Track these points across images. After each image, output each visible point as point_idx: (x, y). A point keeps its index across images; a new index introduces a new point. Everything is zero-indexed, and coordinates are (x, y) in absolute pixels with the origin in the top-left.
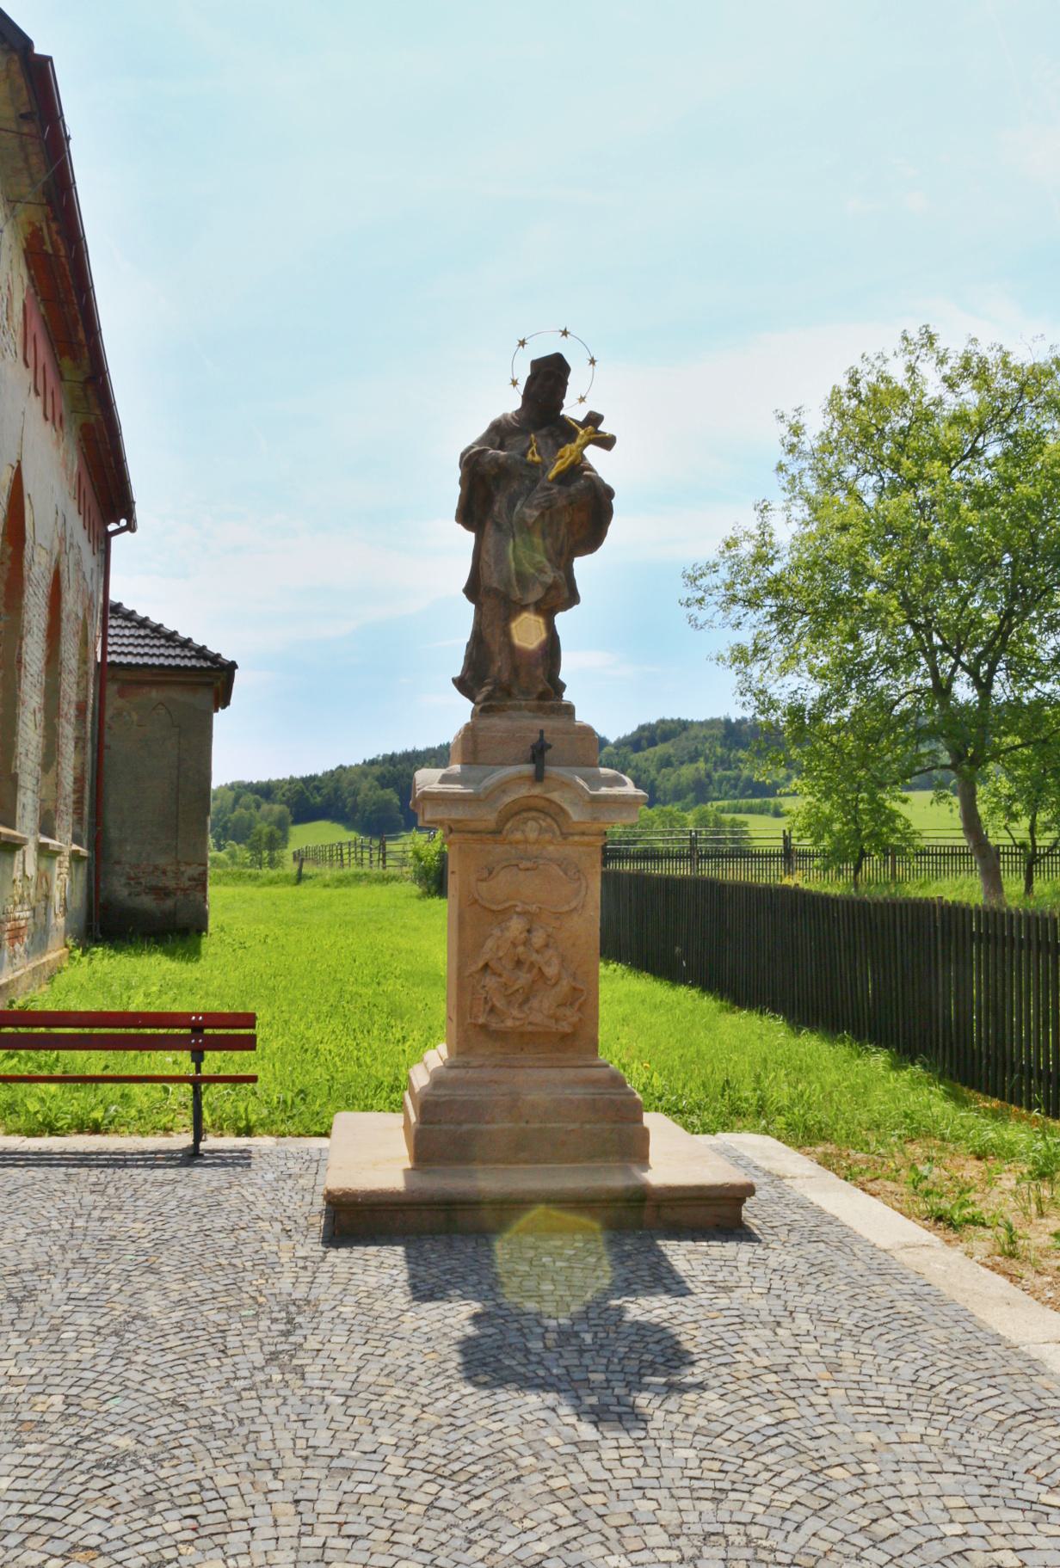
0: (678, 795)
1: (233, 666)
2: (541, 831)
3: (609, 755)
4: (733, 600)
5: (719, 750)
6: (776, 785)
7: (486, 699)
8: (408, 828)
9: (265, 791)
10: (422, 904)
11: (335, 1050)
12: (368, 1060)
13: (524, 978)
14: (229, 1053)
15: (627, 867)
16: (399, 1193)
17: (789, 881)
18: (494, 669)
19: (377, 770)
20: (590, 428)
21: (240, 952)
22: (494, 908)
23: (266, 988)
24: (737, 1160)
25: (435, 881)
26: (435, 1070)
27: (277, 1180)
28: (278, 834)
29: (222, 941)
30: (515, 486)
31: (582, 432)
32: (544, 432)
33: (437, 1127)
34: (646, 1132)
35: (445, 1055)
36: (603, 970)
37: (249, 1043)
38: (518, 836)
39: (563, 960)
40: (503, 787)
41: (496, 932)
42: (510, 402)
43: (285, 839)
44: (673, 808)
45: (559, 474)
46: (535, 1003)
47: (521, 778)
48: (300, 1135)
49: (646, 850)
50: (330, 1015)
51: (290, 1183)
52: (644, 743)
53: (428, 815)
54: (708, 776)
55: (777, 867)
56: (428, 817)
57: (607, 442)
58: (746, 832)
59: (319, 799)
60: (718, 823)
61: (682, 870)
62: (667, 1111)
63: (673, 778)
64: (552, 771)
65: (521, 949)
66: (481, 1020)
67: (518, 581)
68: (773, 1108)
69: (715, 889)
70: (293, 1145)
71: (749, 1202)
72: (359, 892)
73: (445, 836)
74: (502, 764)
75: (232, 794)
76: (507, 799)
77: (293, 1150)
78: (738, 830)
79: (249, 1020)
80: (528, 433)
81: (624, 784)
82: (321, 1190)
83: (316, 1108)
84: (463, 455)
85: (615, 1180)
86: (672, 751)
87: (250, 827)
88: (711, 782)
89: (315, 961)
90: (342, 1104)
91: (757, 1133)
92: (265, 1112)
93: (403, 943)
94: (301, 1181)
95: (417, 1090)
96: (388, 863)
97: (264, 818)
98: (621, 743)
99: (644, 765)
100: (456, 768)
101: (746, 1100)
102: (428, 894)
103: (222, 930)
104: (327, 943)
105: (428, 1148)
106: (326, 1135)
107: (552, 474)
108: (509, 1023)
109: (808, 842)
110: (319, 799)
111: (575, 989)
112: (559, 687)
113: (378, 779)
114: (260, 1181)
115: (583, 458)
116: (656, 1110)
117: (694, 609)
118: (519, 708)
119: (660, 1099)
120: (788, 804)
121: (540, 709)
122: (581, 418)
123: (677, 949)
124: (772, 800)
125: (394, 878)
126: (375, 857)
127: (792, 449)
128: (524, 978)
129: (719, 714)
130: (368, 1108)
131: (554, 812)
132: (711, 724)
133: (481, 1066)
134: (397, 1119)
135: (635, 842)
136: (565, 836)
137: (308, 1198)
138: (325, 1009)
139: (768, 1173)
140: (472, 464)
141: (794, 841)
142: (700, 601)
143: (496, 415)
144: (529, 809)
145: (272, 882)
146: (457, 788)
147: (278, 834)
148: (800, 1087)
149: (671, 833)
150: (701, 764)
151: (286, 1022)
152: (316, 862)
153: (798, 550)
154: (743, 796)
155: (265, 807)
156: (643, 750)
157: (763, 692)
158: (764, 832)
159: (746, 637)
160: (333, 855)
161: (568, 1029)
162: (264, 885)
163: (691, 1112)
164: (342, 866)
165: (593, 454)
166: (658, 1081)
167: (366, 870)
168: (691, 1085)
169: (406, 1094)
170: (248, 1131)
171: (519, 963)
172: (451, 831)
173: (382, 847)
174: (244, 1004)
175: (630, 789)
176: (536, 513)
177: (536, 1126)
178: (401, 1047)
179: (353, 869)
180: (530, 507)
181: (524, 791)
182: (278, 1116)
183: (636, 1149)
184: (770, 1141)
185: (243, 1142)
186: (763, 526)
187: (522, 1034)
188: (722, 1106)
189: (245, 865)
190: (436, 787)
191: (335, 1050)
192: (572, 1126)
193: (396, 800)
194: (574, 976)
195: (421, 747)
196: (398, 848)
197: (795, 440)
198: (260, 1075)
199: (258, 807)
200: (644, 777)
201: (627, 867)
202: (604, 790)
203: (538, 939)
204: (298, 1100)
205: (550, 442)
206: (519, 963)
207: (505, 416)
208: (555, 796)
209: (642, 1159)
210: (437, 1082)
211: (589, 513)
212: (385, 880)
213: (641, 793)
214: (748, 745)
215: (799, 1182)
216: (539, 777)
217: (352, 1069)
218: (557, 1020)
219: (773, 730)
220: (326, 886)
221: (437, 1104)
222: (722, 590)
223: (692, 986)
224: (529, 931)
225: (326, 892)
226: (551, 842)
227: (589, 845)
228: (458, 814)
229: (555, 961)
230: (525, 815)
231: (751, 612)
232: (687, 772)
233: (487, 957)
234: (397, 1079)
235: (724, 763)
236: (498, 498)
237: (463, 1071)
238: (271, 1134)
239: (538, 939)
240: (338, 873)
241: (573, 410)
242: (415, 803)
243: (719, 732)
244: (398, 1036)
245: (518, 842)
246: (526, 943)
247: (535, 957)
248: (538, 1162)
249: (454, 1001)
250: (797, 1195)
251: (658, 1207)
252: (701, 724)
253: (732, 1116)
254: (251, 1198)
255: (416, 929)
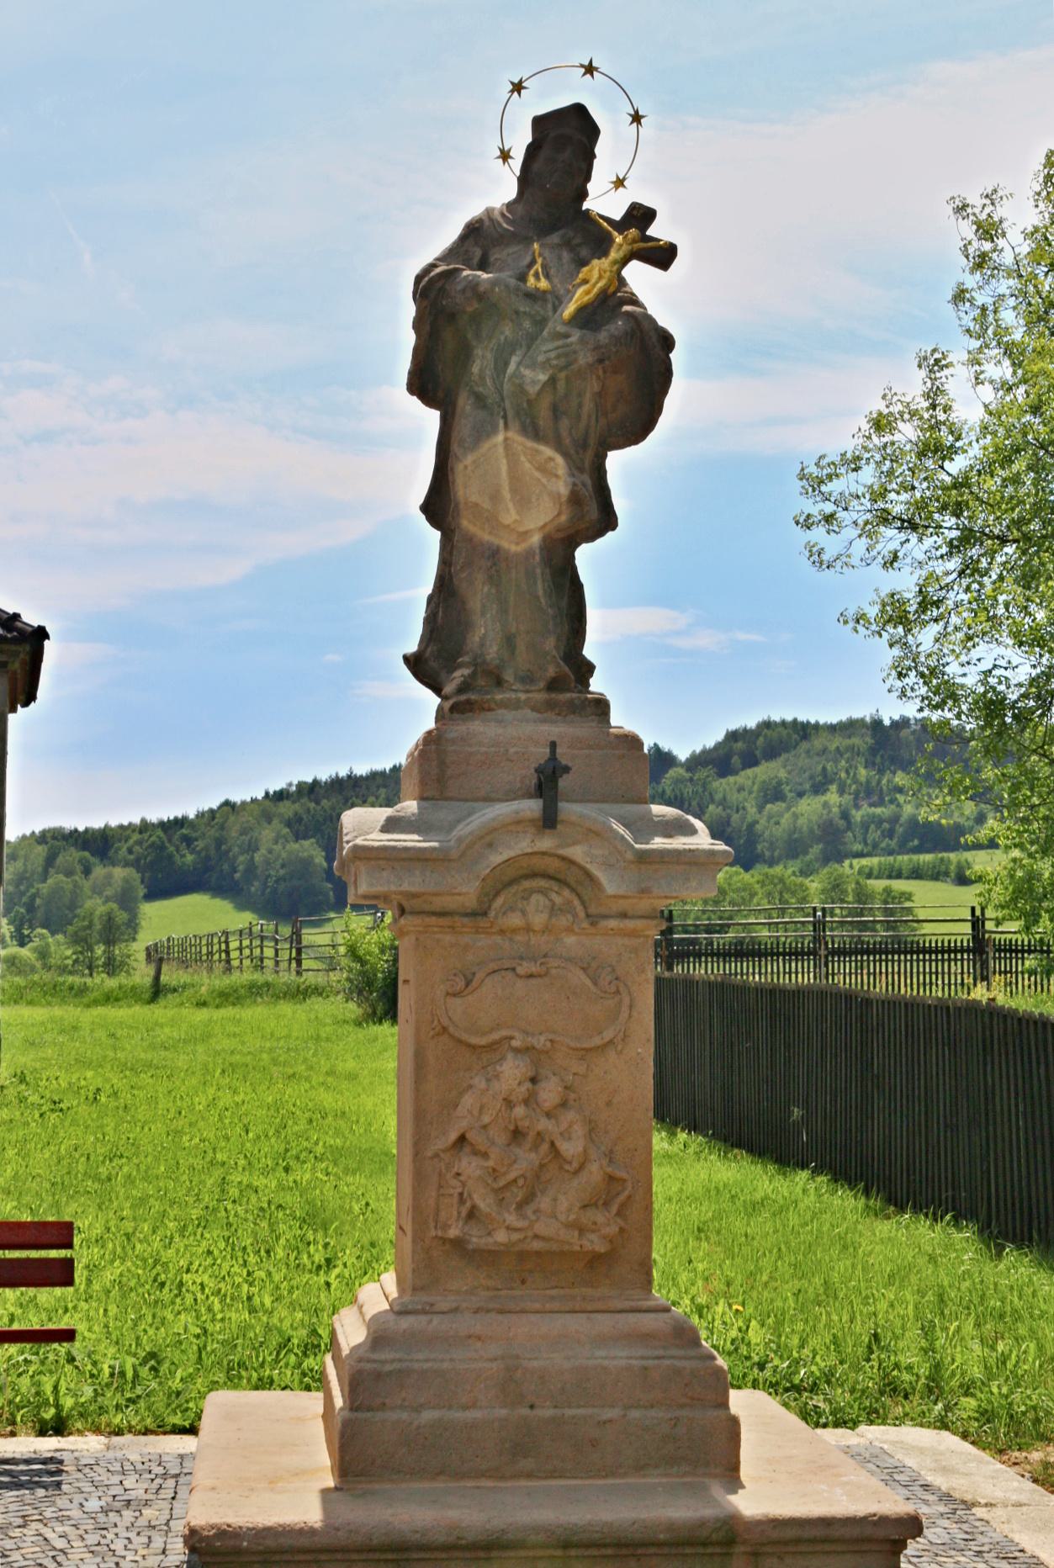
0: (794, 848)
1: (41, 634)
2: (553, 910)
3: (678, 781)
4: (885, 518)
5: (863, 773)
6: (959, 830)
7: (461, 690)
8: (340, 904)
9: (99, 843)
10: (361, 1034)
11: (211, 1284)
12: (268, 1301)
13: (526, 1159)
14: (31, 1291)
15: (701, 970)
16: (312, 1531)
17: (980, 993)
18: (474, 639)
19: (287, 809)
20: (633, 232)
21: (53, 1118)
22: (474, 1040)
23: (96, 1178)
24: (892, 1474)
25: (380, 997)
26: (375, 1317)
27: (105, 1511)
28: (122, 916)
29: (22, 1100)
30: (507, 331)
31: (619, 239)
32: (555, 238)
33: (379, 1416)
34: (734, 1423)
35: (393, 1292)
36: (660, 1141)
37: (62, 1274)
38: (515, 920)
39: (592, 1131)
40: (488, 838)
41: (479, 1082)
42: (499, 188)
43: (133, 926)
44: (786, 871)
45: (581, 310)
46: (544, 1202)
47: (517, 824)
48: (147, 1432)
49: (741, 942)
50: (204, 1224)
51: (128, 1515)
52: (736, 761)
53: (362, 885)
54: (845, 815)
55: (960, 968)
56: (363, 888)
57: (663, 256)
58: (909, 910)
59: (190, 858)
60: (862, 896)
61: (803, 976)
62: (773, 1387)
63: (786, 820)
64: (569, 810)
65: (520, 1111)
66: (453, 1233)
67: (514, 491)
68: (954, 1383)
69: (855, 1004)
70: (135, 1448)
71: (912, 1547)
72: (254, 1013)
73: (395, 920)
74: (488, 799)
75: (41, 851)
76: (496, 858)
77: (135, 1457)
78: (897, 911)
79: (63, 1234)
80: (528, 241)
81: (693, 831)
82: (179, 1527)
83: (176, 1384)
84: (418, 279)
85: (669, 1507)
86: (782, 774)
87: (73, 906)
88: (849, 826)
89: (178, 1133)
90: (220, 1377)
91: (929, 1425)
92: (88, 1392)
93: (328, 1100)
94: (147, 1512)
95: (345, 1351)
96: (306, 964)
97: (97, 891)
98: (698, 761)
99: (734, 797)
100: (410, 806)
101: (909, 1368)
102: (375, 1017)
103: (23, 1080)
104: (201, 1102)
105: (357, 1458)
106: (192, 1430)
107: (569, 310)
108: (501, 1236)
109: (1014, 926)
110: (190, 858)
111: (611, 1178)
112: (586, 670)
113: (289, 824)
114: (75, 1513)
115: (622, 282)
116: (755, 1385)
117: (818, 534)
118: (516, 705)
119: (762, 1366)
120: (981, 862)
121: (550, 706)
122: (617, 215)
123: (797, 1112)
124: (953, 856)
125: (318, 991)
126: (284, 955)
127: (981, 262)
128: (526, 1159)
129: (862, 711)
130: (264, 1384)
131: (568, 878)
132: (849, 727)
133: (455, 1310)
134: (315, 1401)
135: (723, 929)
136: (594, 920)
137: (158, 1543)
138: (195, 1213)
139: (946, 1497)
140: (432, 291)
141: (990, 926)
142: (829, 519)
143: (473, 210)
144: (534, 875)
145: (109, 999)
146: (410, 840)
147: (122, 916)
148: (1000, 1347)
149: (782, 912)
150: (832, 796)
151: (128, 1236)
152: (184, 964)
153: (994, 433)
154: (903, 849)
155: (99, 871)
156: (735, 772)
157: (933, 671)
158: (939, 910)
159: (905, 582)
160: (209, 952)
161: (601, 1247)
162: (96, 1003)
163: (814, 1389)
164: (229, 969)
165: (638, 275)
166: (756, 1335)
167: (269, 977)
168: (814, 1342)
169: (328, 1358)
170: (59, 1427)
171: (517, 1134)
172: (402, 911)
173: (296, 938)
174: (56, 1205)
175: (702, 840)
176: (543, 377)
177: (549, 1413)
178: (322, 1279)
179: (248, 976)
180: (533, 366)
181: (524, 844)
182: (110, 1399)
183: (720, 1455)
184: (949, 1441)
185: (48, 1445)
186: (934, 395)
187: (523, 1256)
188: (868, 1378)
189: (63, 970)
190: (378, 839)
191: (211, 1284)
192: (609, 1414)
193: (319, 859)
194: (610, 1156)
195: (361, 770)
196: (324, 939)
197: (987, 246)
198: (81, 1328)
199: (87, 871)
200: (735, 817)
201: (701, 970)
202: (659, 843)
203: (549, 1093)
204: (144, 1372)
205: (566, 256)
206: (517, 1134)
207: (489, 211)
208: (577, 852)
209: (731, 1476)
210: (379, 1337)
211: (634, 374)
212: (301, 994)
213: (721, 846)
214: (912, 762)
215: (999, 1513)
216: (549, 820)
217: (239, 1315)
218: (582, 1231)
219: (945, 740)
220: (202, 1004)
221: (378, 1376)
222: (866, 502)
223: (816, 1171)
224: (534, 1080)
225: (203, 1015)
226: (569, 930)
227: (633, 934)
228: (412, 883)
229: (579, 1131)
230: (527, 884)
231: (914, 538)
232: (809, 809)
233: (464, 1124)
234: (314, 1332)
235: (869, 793)
236: (479, 352)
237: (423, 1318)
238: (97, 1431)
239: (549, 1093)
240: (222, 982)
241: (604, 201)
242: (343, 865)
243: (862, 742)
244: (319, 1258)
245: (514, 931)
246: (529, 1100)
247: (544, 1124)
248: (553, 1474)
249: (408, 1201)
250: (997, 1537)
251: (756, 1554)
252: (832, 729)
253: (885, 1398)
254: (60, 1544)
255: (352, 1077)
